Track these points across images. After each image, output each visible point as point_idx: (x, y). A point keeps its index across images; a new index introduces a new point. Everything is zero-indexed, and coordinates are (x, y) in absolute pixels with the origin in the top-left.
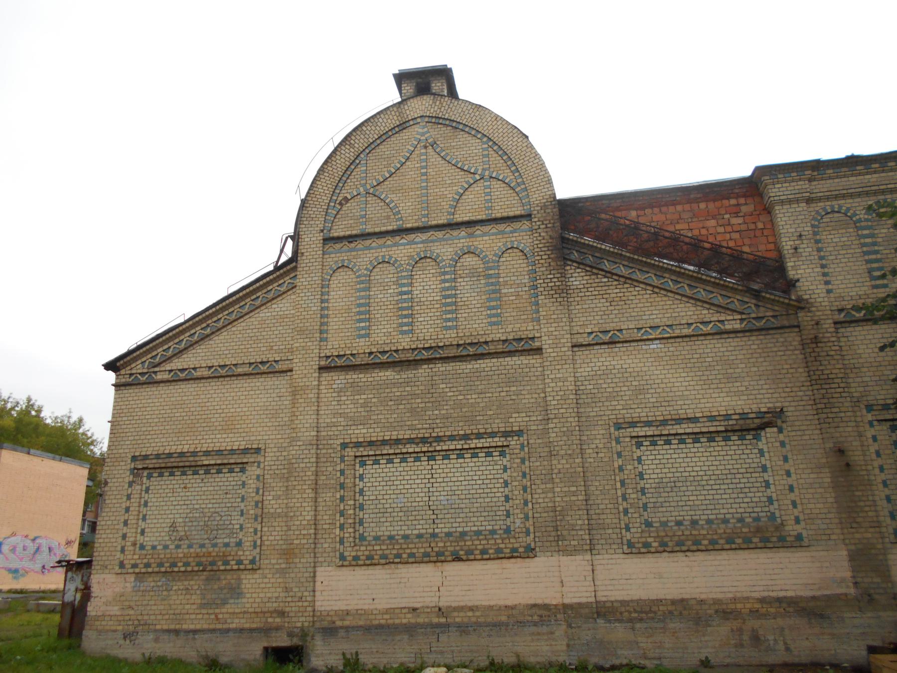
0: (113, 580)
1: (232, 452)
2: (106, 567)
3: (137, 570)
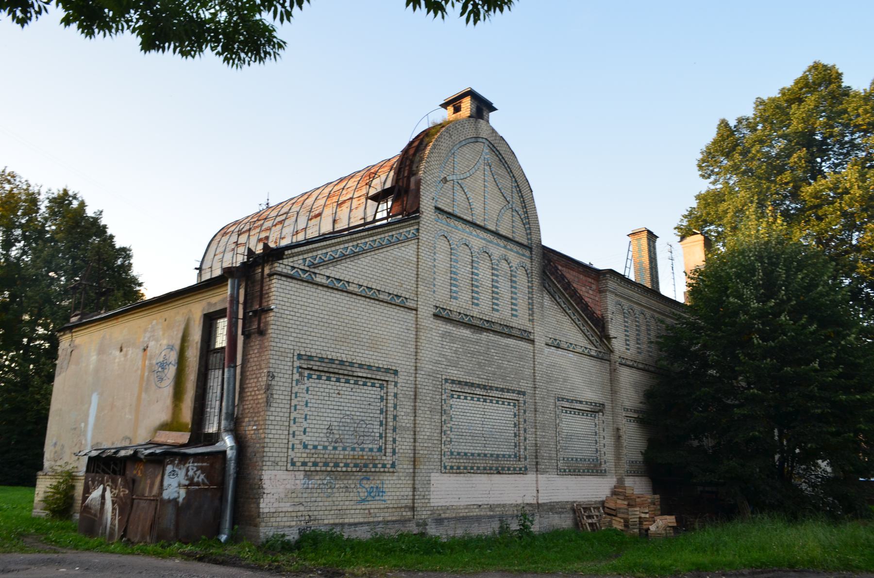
0: (284, 477)
1: (378, 369)
2: (277, 464)
3: (307, 468)
